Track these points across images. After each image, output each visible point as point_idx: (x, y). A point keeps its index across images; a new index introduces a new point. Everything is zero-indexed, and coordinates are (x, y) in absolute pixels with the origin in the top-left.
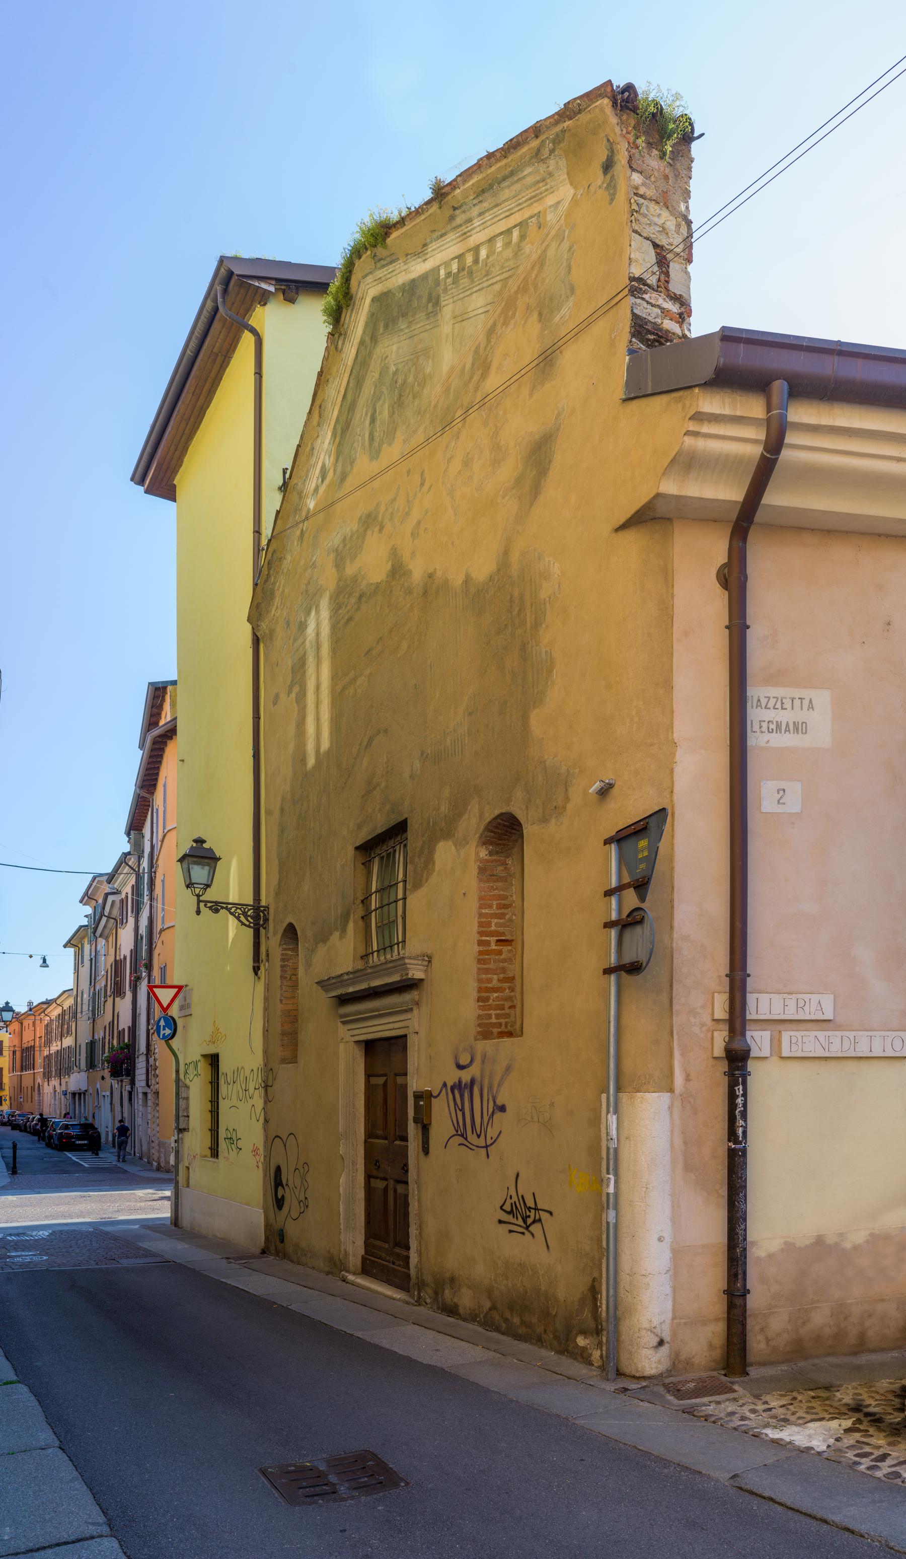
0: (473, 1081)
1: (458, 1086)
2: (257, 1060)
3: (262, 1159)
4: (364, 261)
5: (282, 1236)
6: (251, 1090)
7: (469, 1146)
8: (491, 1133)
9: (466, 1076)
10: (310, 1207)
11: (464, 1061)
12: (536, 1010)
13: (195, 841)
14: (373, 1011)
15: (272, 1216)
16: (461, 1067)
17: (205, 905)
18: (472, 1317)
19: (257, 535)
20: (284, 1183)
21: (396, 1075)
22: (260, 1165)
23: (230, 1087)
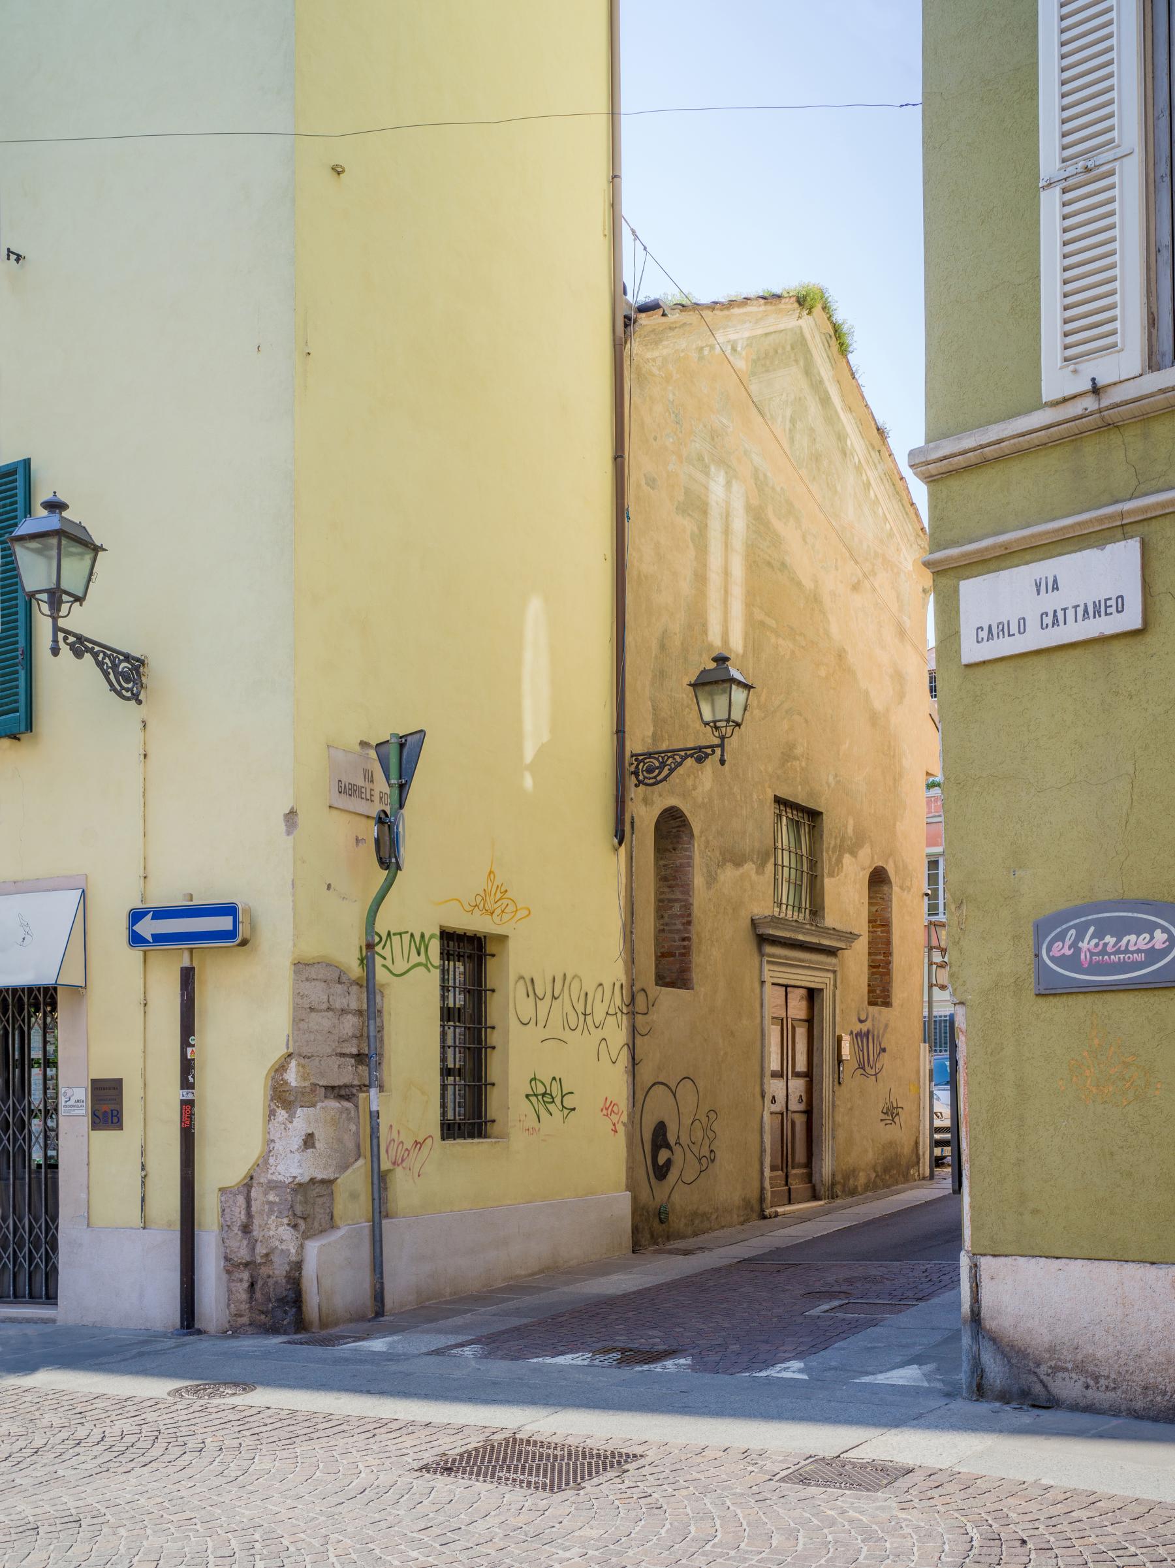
0: (868, 1031)
1: (859, 1035)
2: (616, 972)
3: (624, 1118)
4: (684, 795)
5: (662, 1215)
6: (599, 1016)
7: (866, 1075)
8: (878, 1066)
9: (864, 1027)
10: (717, 1162)
11: (863, 1018)
12: (899, 994)
13: (715, 660)
14: (800, 960)
15: (645, 1194)
16: (861, 1021)
17: (65, 639)
18: (867, 1188)
19: (617, 173)
20: (672, 1140)
21: (812, 995)
22: (621, 1129)
23: (543, 1006)
